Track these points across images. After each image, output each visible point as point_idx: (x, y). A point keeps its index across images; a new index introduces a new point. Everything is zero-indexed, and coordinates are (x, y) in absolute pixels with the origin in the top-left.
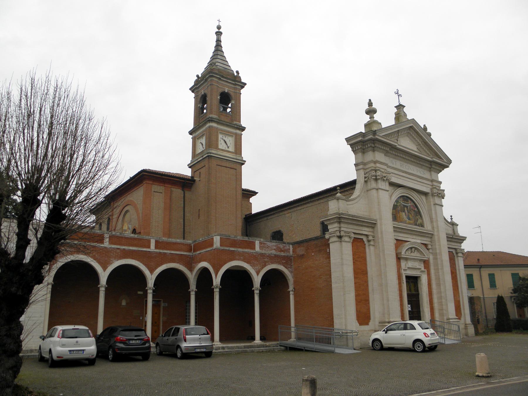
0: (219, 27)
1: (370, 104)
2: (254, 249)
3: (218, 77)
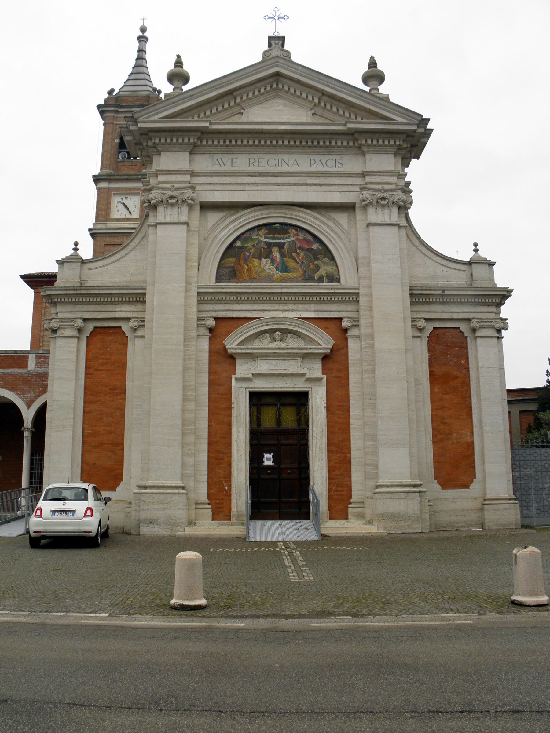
0: (143, 30)
1: (179, 63)
2: (26, 367)
3: (112, 109)
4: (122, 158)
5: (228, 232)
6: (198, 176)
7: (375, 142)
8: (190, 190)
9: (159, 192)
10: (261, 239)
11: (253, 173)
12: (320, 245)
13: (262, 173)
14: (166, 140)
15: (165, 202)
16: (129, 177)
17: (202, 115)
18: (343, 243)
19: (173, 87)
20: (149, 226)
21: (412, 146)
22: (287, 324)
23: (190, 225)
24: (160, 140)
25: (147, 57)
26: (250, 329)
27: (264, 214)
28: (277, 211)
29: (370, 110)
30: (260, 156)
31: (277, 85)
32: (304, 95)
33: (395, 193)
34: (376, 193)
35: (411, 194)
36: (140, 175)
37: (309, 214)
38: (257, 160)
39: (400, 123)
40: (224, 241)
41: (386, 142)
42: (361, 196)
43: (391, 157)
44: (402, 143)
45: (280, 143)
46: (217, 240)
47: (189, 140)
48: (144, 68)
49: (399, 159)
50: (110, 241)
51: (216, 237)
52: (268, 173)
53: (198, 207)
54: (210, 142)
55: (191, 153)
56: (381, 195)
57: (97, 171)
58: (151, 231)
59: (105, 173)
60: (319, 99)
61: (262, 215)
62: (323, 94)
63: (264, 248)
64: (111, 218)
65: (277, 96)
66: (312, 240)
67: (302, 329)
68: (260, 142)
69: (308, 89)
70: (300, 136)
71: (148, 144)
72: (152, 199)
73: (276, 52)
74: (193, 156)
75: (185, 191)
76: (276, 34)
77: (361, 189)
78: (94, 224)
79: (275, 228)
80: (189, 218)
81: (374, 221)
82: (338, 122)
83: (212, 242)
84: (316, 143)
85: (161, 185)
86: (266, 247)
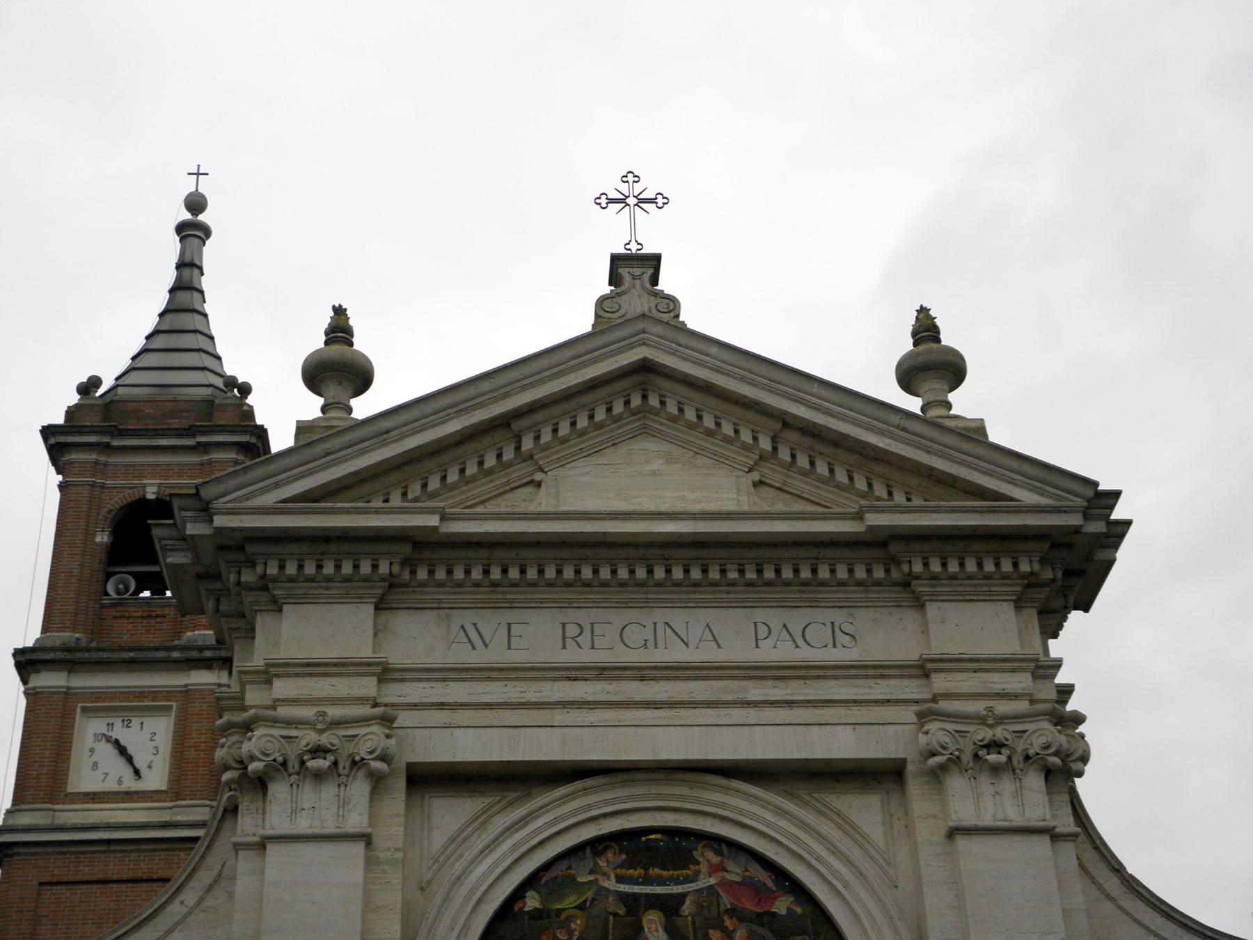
0: (196, 204)
1: (339, 330)
3: (93, 439)
4: (118, 592)
5: (496, 864)
6: (403, 680)
7: (953, 567)
8: (375, 728)
9: (277, 732)
10: (606, 884)
11: (577, 669)
12: (798, 901)
13: (604, 669)
14: (301, 567)
15: (293, 764)
16: (140, 655)
17: (415, 490)
18: (873, 893)
19: (320, 401)
20: (237, 847)
21: (1068, 573)
23: (376, 841)
24: (282, 567)
25: (206, 283)
27: (614, 801)
28: (654, 790)
29: (932, 469)
30: (595, 614)
31: (645, 397)
32: (727, 429)
33: (1030, 727)
34: (971, 728)
35: (1081, 729)
36: (176, 648)
37: (756, 797)
38: (587, 628)
39: (1029, 508)
40: (484, 894)
41: (989, 567)
42: (923, 739)
43: (1008, 608)
44: (1037, 567)
45: (659, 573)
46: (464, 890)
47: (375, 567)
48: (197, 317)
49: (1031, 615)
50: (59, 868)
51: (458, 879)
52: (625, 669)
53: (402, 783)
54: (441, 574)
55: (378, 608)
56: (985, 734)
57: (30, 634)
58: (245, 862)
59: (58, 643)
60: (774, 440)
61: (606, 803)
62: (785, 425)
63: (615, 915)
64: (70, 789)
65: (645, 431)
66: (770, 884)
68: (596, 572)
69: (739, 411)
70: (720, 552)
71: (243, 579)
72: (253, 758)
73: (635, 303)
74: (385, 616)
75: (361, 731)
76: (634, 247)
77: (920, 715)
78: (8, 812)
79: (651, 848)
80: (372, 818)
81: (970, 820)
82: (837, 510)
83: (447, 898)
84: (769, 574)
85: (282, 711)
86: (621, 911)
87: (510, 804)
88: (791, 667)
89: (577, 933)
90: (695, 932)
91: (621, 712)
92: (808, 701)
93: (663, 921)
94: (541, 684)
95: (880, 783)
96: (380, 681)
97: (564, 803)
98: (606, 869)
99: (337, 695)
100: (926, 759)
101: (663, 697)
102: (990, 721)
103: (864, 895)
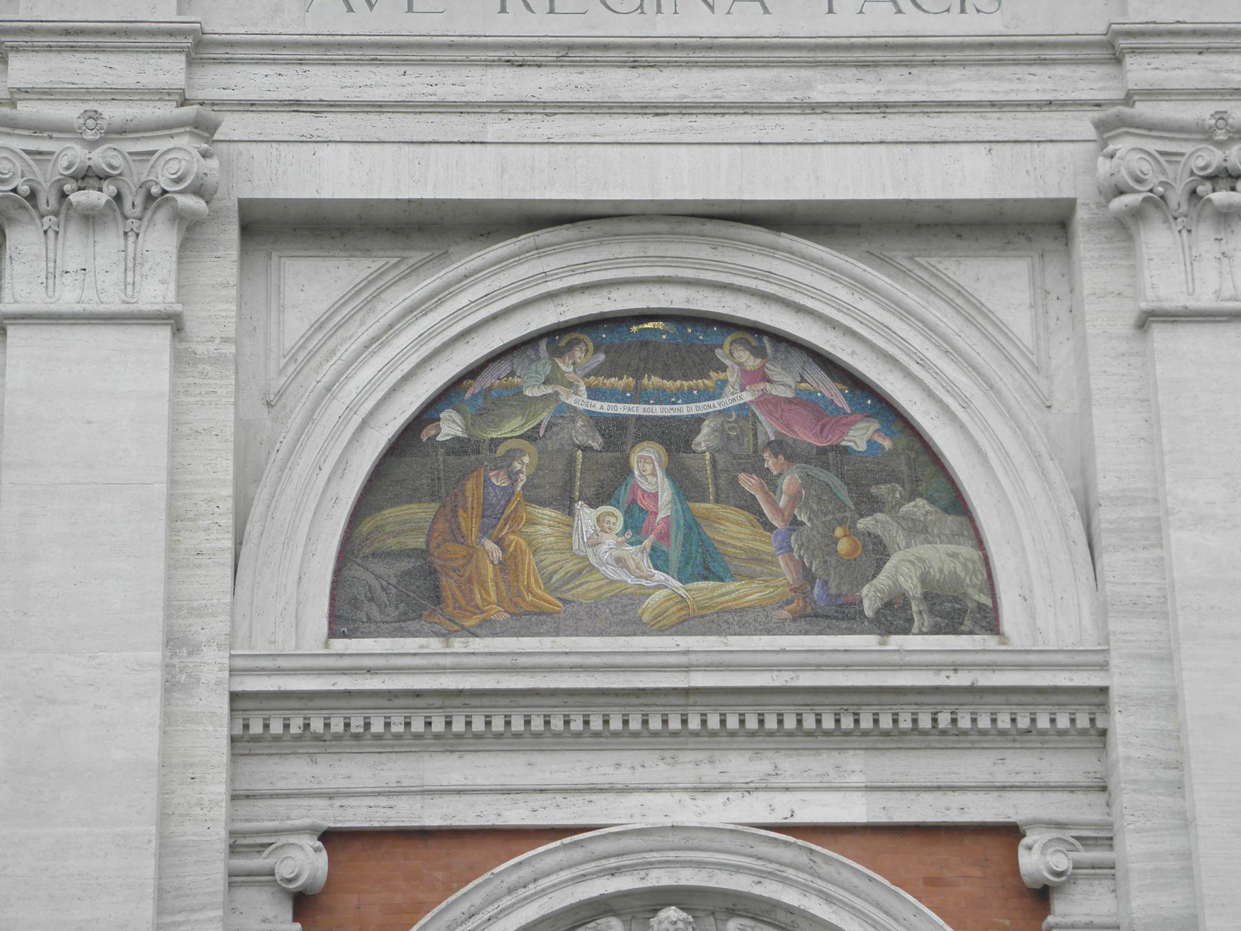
5: (391, 365)
6: (229, 62)
8: (184, 141)
10: (571, 401)
12: (887, 431)
13: (570, 47)
15: (47, 199)
18: (1010, 415)
22: (720, 866)
23: (190, 326)
26: (522, 893)
27: (585, 267)
28: (654, 249)
37: (821, 262)
42: (1104, 166)
46: (337, 407)
51: (328, 389)
52: (606, 47)
53: (233, 233)
56: (1212, 157)
61: (572, 270)
63: (586, 449)
66: (841, 402)
67: (805, 888)
75: (161, 145)
77: (1103, 127)
83: (310, 419)
86: (597, 443)
87: (414, 270)
88: (886, 46)
89: (523, 477)
90: (715, 477)
91: (598, 120)
92: (915, 104)
93: (665, 459)
94: (465, 71)
95: (1029, 239)
96: (191, 62)
97: (502, 270)
98: (572, 377)
99: (119, 83)
100: (1109, 201)
101: (668, 95)
102: (1221, 136)
103: (995, 420)
